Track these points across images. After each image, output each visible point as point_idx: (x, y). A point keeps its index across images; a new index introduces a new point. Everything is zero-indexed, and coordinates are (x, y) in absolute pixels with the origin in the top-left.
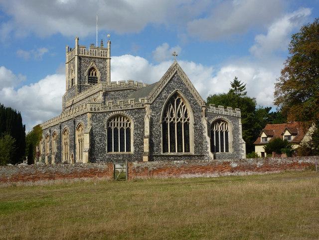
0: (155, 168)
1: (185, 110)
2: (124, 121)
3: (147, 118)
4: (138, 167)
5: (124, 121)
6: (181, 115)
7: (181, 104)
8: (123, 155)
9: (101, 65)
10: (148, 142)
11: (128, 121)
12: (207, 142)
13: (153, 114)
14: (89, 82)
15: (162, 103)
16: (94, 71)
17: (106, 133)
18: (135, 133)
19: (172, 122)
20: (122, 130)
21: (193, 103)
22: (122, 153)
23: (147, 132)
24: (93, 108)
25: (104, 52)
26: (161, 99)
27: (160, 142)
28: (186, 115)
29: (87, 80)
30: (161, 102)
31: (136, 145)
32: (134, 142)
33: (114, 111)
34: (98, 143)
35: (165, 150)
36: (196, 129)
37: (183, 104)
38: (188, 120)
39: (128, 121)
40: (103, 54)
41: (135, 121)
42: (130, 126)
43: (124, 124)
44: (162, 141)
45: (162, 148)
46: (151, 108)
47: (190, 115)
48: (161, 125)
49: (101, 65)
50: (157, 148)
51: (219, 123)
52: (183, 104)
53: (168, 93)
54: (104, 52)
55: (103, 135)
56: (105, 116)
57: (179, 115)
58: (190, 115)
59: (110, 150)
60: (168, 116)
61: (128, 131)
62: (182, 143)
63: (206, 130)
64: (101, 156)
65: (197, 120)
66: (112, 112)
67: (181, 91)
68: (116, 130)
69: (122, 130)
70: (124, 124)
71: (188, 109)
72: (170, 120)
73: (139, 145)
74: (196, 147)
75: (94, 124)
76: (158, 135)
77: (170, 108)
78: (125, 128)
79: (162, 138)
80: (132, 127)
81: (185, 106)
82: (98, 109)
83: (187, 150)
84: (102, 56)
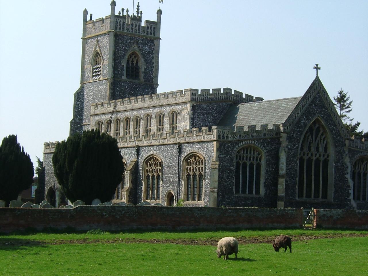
0: (339, 217)
1: (325, 142)
2: (254, 154)
3: (283, 151)
4: (324, 215)
5: (254, 154)
6: (321, 149)
7: (320, 134)
8: (252, 198)
9: (146, 49)
10: (284, 184)
11: (259, 154)
12: (349, 186)
13: (290, 147)
14: (99, 64)
15: (301, 132)
16: (135, 57)
17: (234, 169)
18: (267, 171)
19: (310, 158)
20: (252, 165)
21: (335, 134)
22: (251, 196)
23: (282, 170)
24: (222, 135)
25: (151, 28)
26: (300, 127)
27: (295, 184)
28: (326, 149)
29: (125, 73)
30: (299, 131)
31: (266, 187)
32: (265, 183)
33: (245, 140)
34: (226, 182)
35: (301, 195)
36: (336, 168)
37: (322, 134)
38: (328, 156)
39: (259, 154)
40: (149, 30)
41: (267, 154)
42: (260, 160)
43: (254, 158)
44: (298, 182)
45: (297, 191)
46: (287, 139)
47: (331, 150)
48: (298, 162)
49: (146, 49)
50: (292, 191)
51: (363, 162)
52: (322, 134)
53: (307, 119)
54: (151, 28)
55: (231, 171)
56: (234, 146)
57: (317, 149)
58: (331, 150)
59: (237, 191)
60: (306, 150)
61: (259, 166)
62: (319, 185)
63: (349, 170)
64: (228, 199)
65: (340, 155)
66: (242, 141)
67: (323, 117)
68: (245, 165)
69: (252, 165)
70: (254, 158)
71: (329, 140)
72: (316, 156)
73: (272, 185)
74: (336, 192)
75: (222, 156)
76: (294, 174)
77: (308, 139)
78: (255, 163)
79: (297, 179)
80: (263, 163)
81: (324, 138)
82: (227, 137)
83: (325, 196)
84: (147, 34)
